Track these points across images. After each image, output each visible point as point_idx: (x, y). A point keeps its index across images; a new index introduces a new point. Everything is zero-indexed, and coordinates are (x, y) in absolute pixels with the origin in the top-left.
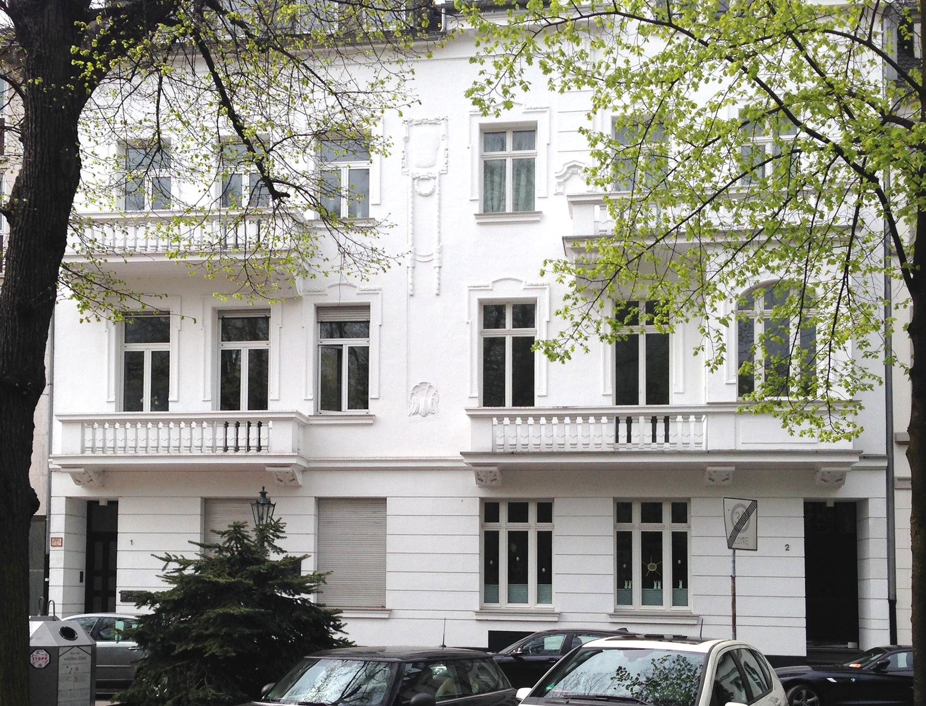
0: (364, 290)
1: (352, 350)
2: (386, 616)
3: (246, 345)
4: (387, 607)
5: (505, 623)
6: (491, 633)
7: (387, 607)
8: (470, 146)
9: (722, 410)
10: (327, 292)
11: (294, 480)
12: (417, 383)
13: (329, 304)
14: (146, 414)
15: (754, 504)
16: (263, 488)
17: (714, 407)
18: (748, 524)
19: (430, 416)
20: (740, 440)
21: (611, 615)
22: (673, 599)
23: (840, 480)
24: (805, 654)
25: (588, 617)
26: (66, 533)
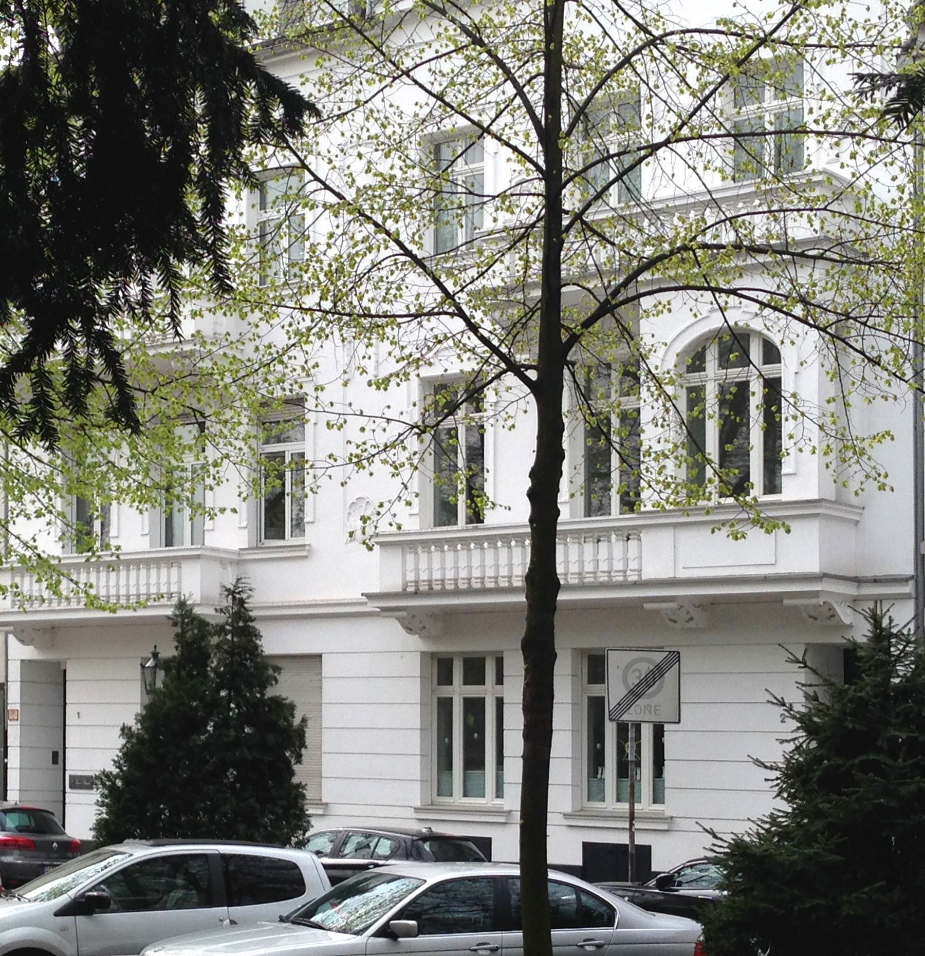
2: (665, 827)
4: (324, 801)
6: (587, 846)
7: (324, 801)
9: (800, 512)
11: (833, 616)
12: (353, 500)
14: (614, 520)
15: (676, 657)
16: (155, 647)
17: (651, 518)
18: (661, 687)
20: (681, 564)
21: (417, 810)
22: (452, 784)
25: (368, 811)
26: (21, 704)
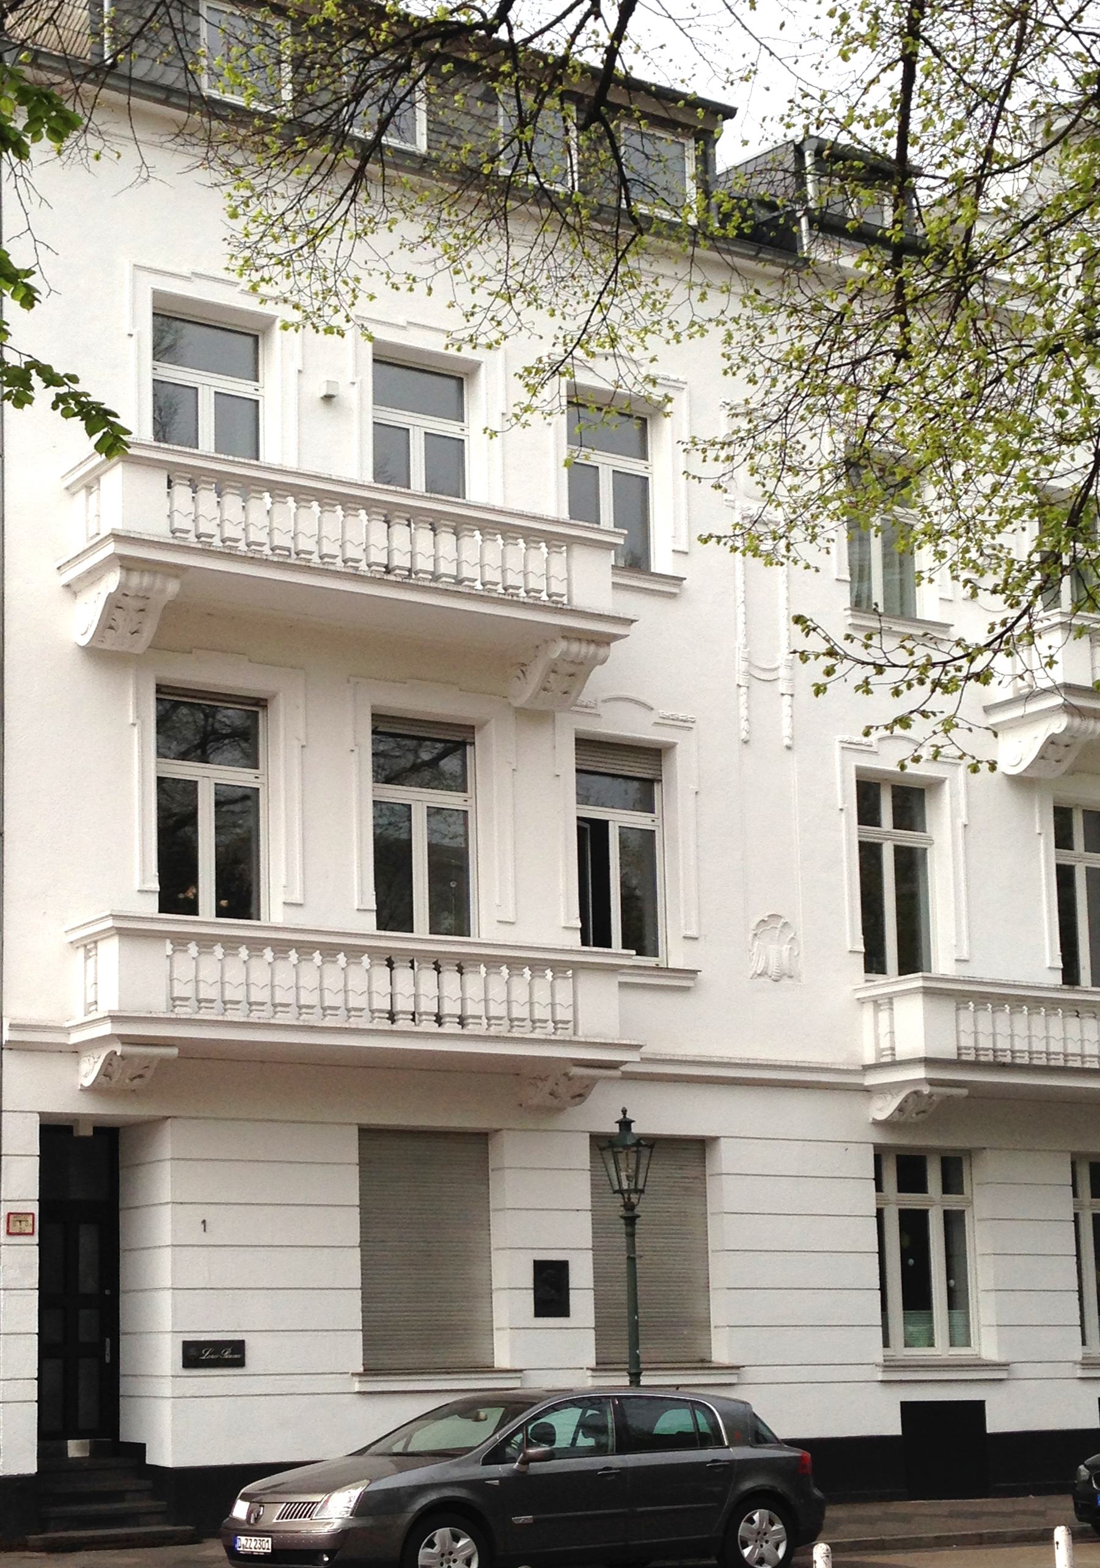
0: (668, 718)
1: (434, 812)
3: (426, 797)
5: (929, 1386)
8: (357, 380)
10: (602, 709)
13: (625, 738)
16: (624, 1112)
19: (786, 981)
23: (580, 1095)
24: (991, 1428)
